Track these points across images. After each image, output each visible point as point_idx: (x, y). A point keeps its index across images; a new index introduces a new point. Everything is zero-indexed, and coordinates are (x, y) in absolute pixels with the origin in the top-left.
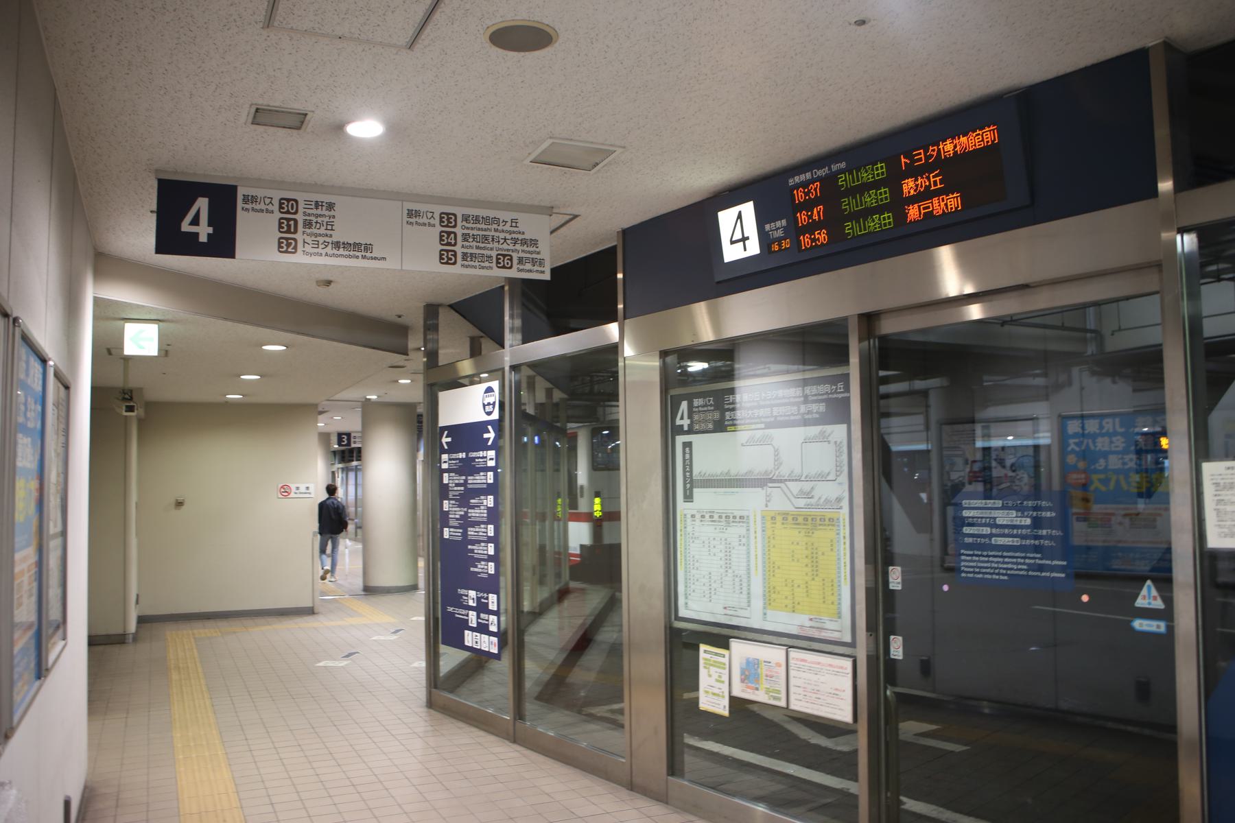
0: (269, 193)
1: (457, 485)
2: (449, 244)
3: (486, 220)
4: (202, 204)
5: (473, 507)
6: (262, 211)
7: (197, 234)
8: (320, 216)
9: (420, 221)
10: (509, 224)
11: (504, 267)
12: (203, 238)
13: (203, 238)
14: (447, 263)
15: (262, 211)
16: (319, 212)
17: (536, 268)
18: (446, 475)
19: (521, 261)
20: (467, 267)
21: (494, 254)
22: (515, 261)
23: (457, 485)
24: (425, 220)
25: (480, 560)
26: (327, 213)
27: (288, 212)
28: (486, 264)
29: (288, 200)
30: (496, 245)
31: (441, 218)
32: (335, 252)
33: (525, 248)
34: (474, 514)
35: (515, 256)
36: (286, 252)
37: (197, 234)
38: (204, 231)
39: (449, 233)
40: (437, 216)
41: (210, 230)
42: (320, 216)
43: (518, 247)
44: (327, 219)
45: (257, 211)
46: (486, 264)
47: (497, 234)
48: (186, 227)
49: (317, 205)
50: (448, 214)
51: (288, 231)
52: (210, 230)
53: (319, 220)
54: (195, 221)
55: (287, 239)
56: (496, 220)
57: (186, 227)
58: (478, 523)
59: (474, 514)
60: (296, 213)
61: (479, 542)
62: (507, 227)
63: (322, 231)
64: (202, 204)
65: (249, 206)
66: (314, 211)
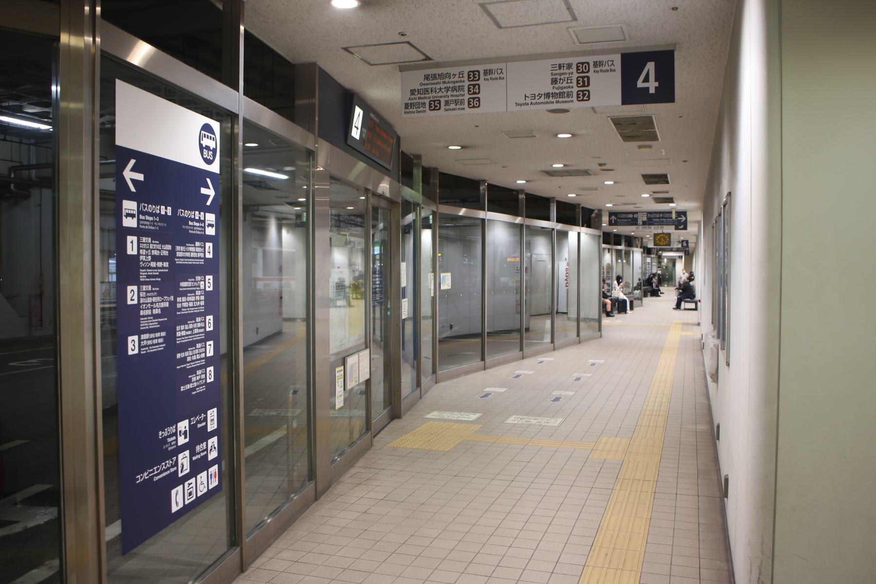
0: (461, 69)
1: (155, 258)
2: (475, 93)
3: (441, 76)
4: (650, 66)
5: (185, 294)
6: (497, 79)
7: (648, 88)
8: (563, 74)
9: (493, 76)
10: (457, 76)
11: (474, 107)
12: (652, 91)
13: (652, 91)
14: (434, 109)
15: (497, 79)
16: (562, 71)
17: (458, 107)
18: (132, 240)
19: (447, 103)
20: (408, 113)
21: (427, 101)
22: (443, 104)
23: (155, 258)
24: (496, 76)
25: (193, 371)
26: (567, 71)
27: (583, 72)
28: (422, 109)
29: (583, 63)
30: (434, 94)
31: (469, 75)
32: (546, 100)
33: (455, 93)
34: (186, 303)
35: (443, 100)
36: (583, 100)
37: (648, 88)
38: (652, 86)
39: (474, 86)
40: (466, 75)
41: (657, 84)
42: (563, 74)
43: (450, 93)
44: (567, 76)
45: (494, 79)
46: (422, 109)
47: (434, 86)
48: (640, 84)
49: (560, 66)
50: (473, 72)
51: (583, 86)
52: (657, 84)
53: (562, 77)
54: (646, 80)
55: (583, 91)
56: (448, 75)
57: (640, 84)
58: (192, 317)
59: (186, 303)
60: (588, 72)
61: (193, 344)
62: (457, 79)
63: (565, 84)
64: (650, 66)
65: (598, 69)
66: (559, 72)
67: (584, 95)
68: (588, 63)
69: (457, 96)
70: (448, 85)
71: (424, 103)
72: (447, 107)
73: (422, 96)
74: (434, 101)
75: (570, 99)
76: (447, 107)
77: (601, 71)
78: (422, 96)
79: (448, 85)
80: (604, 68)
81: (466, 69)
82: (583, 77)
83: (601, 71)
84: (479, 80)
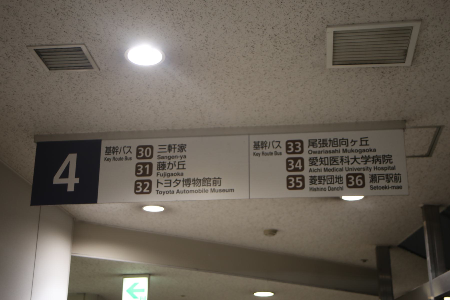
2: (296, 170)
6: (271, 154)
7: (66, 186)
8: (173, 157)
10: (358, 143)
12: (71, 189)
13: (71, 189)
14: (295, 188)
15: (271, 154)
16: (172, 154)
17: (391, 184)
19: (373, 178)
20: (316, 190)
21: (344, 174)
26: (179, 154)
27: (144, 158)
28: (336, 185)
31: (287, 146)
32: (186, 188)
35: (367, 174)
36: (142, 193)
37: (66, 186)
39: (296, 160)
40: (283, 145)
41: (77, 181)
42: (173, 157)
43: (370, 164)
44: (179, 160)
48: (57, 180)
49: (170, 148)
50: (294, 141)
51: (144, 174)
52: (77, 181)
53: (172, 161)
54: (65, 175)
55: (142, 181)
57: (57, 180)
60: (151, 157)
63: (175, 170)
66: (168, 154)
67: (144, 187)
68: (152, 147)
69: (334, 170)
70: (366, 154)
71: (340, 178)
72: (375, 185)
73: (330, 167)
74: (355, 175)
75: (398, 184)
76: (375, 185)
77: (263, 153)
78: (330, 167)
79: (366, 154)
80: (267, 151)
81: (135, 143)
82: (144, 164)
83: (263, 153)
84: (302, 152)
